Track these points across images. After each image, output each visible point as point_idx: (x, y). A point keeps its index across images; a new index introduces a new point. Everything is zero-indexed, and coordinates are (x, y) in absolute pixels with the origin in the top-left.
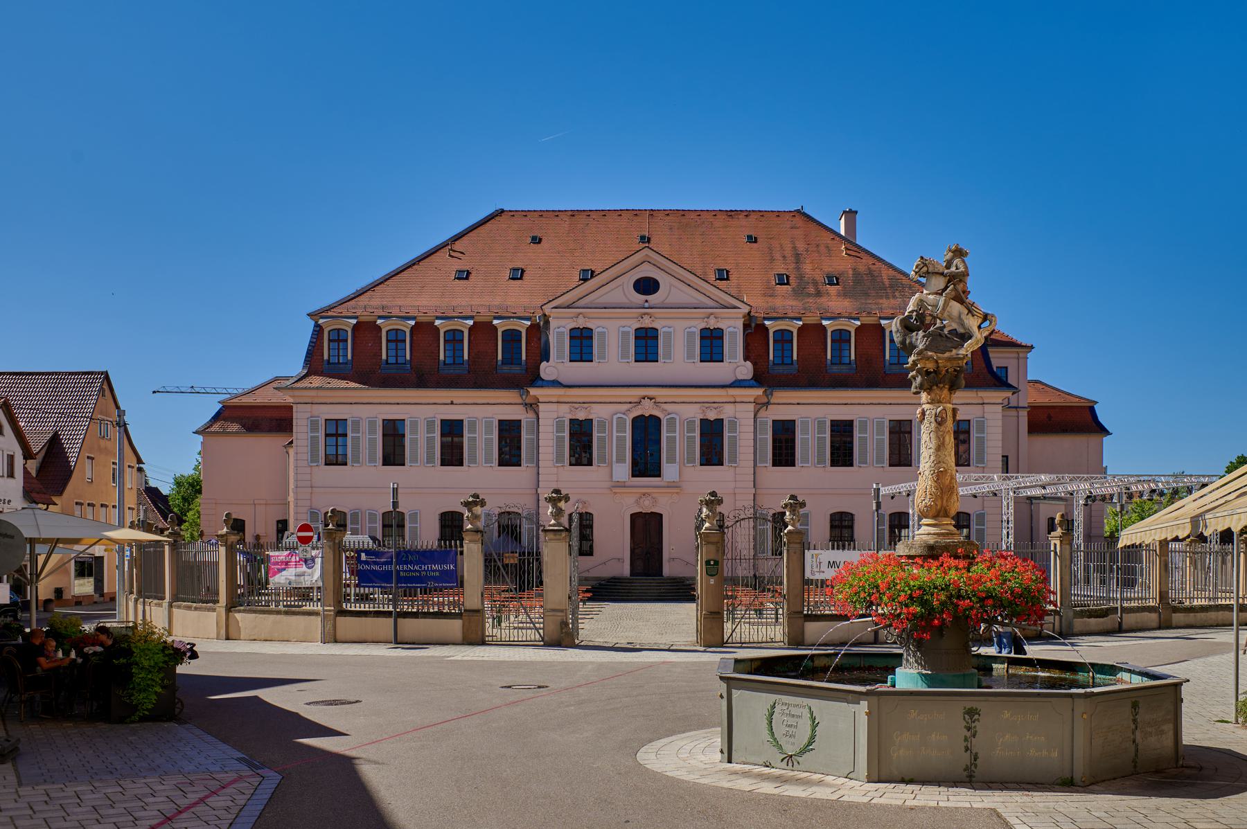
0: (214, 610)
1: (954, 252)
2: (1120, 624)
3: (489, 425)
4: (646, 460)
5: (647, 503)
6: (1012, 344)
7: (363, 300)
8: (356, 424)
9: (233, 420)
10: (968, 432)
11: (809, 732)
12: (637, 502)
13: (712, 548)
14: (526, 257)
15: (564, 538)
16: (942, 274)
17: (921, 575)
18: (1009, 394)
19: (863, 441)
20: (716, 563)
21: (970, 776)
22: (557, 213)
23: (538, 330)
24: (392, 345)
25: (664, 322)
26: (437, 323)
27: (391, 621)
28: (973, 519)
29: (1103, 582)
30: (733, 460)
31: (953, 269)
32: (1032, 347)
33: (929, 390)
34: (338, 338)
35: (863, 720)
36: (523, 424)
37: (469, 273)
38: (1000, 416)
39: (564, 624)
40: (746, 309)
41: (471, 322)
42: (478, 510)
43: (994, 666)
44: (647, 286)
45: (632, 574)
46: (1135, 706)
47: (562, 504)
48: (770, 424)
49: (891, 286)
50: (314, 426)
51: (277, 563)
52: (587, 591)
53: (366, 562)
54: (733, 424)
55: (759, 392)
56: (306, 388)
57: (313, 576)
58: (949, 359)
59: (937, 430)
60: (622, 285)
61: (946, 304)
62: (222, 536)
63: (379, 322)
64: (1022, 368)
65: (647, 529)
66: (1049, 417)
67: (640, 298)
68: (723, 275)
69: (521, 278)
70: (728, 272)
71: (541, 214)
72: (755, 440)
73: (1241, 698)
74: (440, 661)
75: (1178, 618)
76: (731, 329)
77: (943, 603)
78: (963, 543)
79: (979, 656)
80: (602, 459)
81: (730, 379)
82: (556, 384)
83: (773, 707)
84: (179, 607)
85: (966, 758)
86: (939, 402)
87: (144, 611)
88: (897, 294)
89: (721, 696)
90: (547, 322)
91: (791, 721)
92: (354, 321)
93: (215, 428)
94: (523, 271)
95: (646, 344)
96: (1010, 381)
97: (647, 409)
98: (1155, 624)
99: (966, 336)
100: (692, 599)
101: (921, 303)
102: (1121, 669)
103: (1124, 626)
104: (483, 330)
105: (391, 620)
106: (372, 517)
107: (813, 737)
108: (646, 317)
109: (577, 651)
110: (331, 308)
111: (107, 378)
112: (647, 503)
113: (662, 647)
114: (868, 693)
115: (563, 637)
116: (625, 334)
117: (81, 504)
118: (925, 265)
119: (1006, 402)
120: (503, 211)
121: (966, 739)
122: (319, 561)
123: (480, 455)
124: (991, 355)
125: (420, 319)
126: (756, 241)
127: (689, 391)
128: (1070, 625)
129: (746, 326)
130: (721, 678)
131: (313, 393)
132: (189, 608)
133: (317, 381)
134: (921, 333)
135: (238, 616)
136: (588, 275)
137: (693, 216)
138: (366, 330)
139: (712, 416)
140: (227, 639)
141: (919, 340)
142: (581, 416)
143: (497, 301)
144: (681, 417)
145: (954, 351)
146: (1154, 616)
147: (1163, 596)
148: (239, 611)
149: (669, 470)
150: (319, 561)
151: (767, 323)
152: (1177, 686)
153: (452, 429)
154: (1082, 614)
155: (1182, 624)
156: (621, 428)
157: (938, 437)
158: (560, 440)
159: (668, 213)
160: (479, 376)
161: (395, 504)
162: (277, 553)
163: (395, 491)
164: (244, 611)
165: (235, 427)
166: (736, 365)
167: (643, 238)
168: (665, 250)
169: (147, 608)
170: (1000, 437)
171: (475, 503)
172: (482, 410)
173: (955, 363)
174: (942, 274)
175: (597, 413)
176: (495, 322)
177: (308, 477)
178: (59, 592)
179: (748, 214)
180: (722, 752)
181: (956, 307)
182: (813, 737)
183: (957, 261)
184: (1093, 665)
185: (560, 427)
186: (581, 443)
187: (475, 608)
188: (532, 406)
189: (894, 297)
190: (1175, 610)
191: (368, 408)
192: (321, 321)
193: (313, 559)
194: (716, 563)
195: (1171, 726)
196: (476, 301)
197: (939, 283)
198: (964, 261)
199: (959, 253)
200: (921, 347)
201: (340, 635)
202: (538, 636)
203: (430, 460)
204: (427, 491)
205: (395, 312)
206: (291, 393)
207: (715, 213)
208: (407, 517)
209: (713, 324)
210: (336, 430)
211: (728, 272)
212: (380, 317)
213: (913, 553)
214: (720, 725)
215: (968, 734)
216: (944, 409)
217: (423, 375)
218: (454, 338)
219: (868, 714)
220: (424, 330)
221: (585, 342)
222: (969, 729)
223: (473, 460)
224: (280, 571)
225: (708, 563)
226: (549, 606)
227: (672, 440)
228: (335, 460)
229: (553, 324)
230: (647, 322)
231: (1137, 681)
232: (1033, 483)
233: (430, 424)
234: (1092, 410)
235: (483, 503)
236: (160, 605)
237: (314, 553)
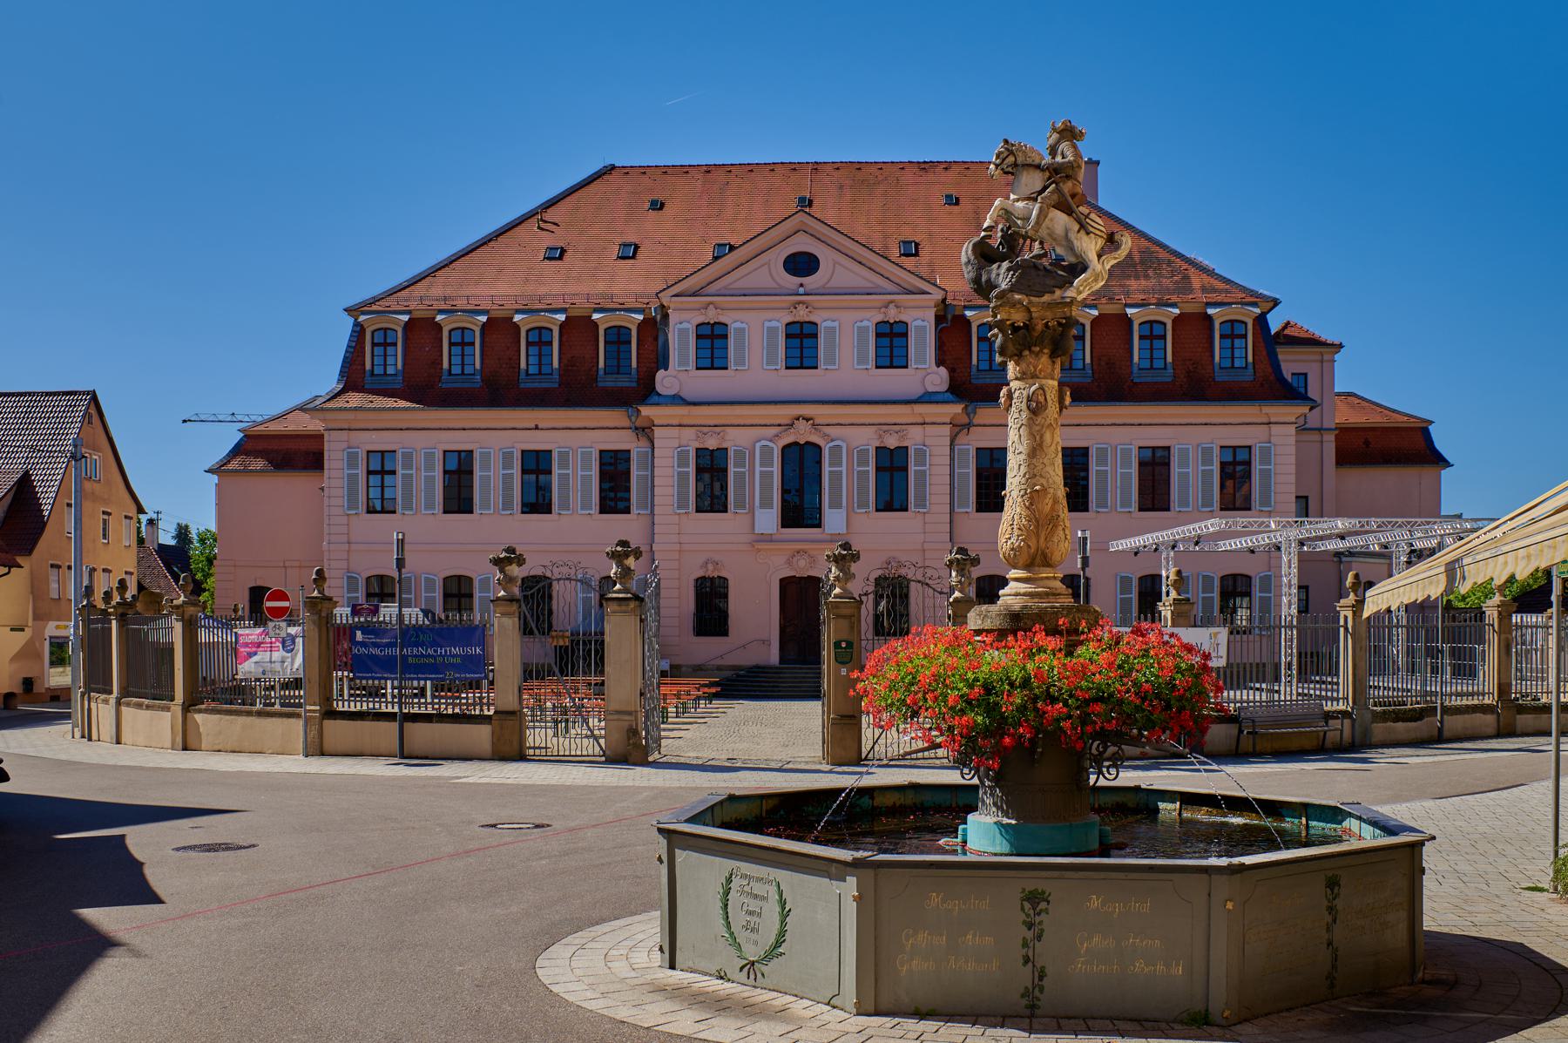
0: (168, 709)
1: (1061, 132)
2: (1440, 730)
3: (586, 457)
4: (799, 509)
5: (802, 563)
6: (1313, 342)
7: (419, 290)
8: (408, 457)
9: (257, 454)
10: (1248, 463)
11: (777, 926)
12: (789, 562)
13: (844, 623)
14: (646, 230)
15: (633, 610)
16: (1038, 167)
17: (995, 660)
18: (1305, 410)
19: (1102, 476)
20: (850, 644)
21: (1033, 1007)
22: (685, 170)
23: (654, 328)
24: (457, 350)
25: (825, 314)
26: (517, 318)
27: (395, 726)
28: (1256, 583)
29: (1435, 670)
30: (921, 502)
31: (1059, 159)
32: (1341, 346)
33: (1018, 357)
34: (384, 342)
35: (851, 908)
36: (634, 456)
37: (563, 251)
38: (1292, 440)
39: (633, 732)
40: (939, 295)
41: (562, 317)
42: (514, 570)
43: (1162, 805)
44: (802, 264)
45: (781, 661)
46: (1333, 883)
47: (631, 562)
48: (972, 453)
49: (1142, 262)
50: (352, 460)
51: (246, 645)
52: (711, 685)
53: (363, 644)
54: (921, 454)
55: (957, 409)
56: (340, 409)
57: (294, 663)
58: (1049, 306)
59: (1030, 424)
60: (768, 263)
61: (1042, 214)
62: (177, 607)
63: (439, 318)
64: (1327, 375)
65: (800, 596)
66: (1367, 443)
67: (792, 281)
68: (911, 250)
69: (634, 257)
70: (917, 245)
71: (666, 170)
72: (952, 475)
73: (1562, 853)
74: (439, 782)
75: (1524, 720)
76: (919, 323)
77: (1022, 709)
78: (1069, 609)
79: (1097, 790)
80: (740, 504)
81: (916, 390)
82: (678, 400)
83: (729, 880)
84: (128, 705)
85: (1025, 976)
86: (1034, 376)
87: (89, 710)
88: (1150, 272)
89: (660, 859)
90: (666, 316)
91: (754, 905)
92: (406, 318)
93: (234, 465)
94: (637, 247)
95: (802, 343)
96: (1310, 394)
97: (803, 433)
98: (1491, 731)
99: (1079, 267)
100: (814, 694)
101: (1007, 214)
102: (1350, 815)
103: (1446, 734)
104: (578, 327)
105: (395, 726)
106: (430, 584)
107: (782, 933)
108: (800, 307)
109: (646, 770)
110: (375, 300)
111: (94, 399)
112: (802, 563)
113: (773, 765)
114: (857, 864)
115: (631, 750)
116: (772, 331)
117: (59, 567)
118: (1011, 153)
119: (1301, 421)
120: (613, 167)
121: (1025, 944)
122: (299, 641)
123: (576, 498)
124: (1280, 357)
125: (494, 314)
126: (957, 203)
127: (863, 401)
128: (1366, 732)
129: (939, 319)
130: (660, 830)
131: (350, 416)
132: (139, 706)
133: (355, 399)
134: (1005, 265)
135: (198, 717)
136: (723, 250)
137: (873, 170)
138: (422, 329)
139: (892, 442)
140: (185, 749)
141: (1002, 275)
142: (712, 443)
143: (601, 287)
144: (849, 446)
145: (1058, 293)
146: (1490, 719)
147: (1504, 689)
148: (200, 711)
149: (834, 520)
150: (299, 641)
151: (968, 313)
152: (1415, 848)
153: (536, 464)
154: (1384, 717)
155: (1530, 730)
156: (766, 461)
157: (1032, 435)
158: (683, 477)
159: (838, 166)
160: (575, 389)
161: (400, 563)
162: (247, 631)
163: (401, 543)
164: (206, 711)
165: (259, 464)
166: (925, 371)
167: (802, 200)
168: (831, 216)
169: (93, 705)
170: (1293, 469)
171: (509, 561)
172: (578, 438)
173: (1059, 312)
174: (1038, 167)
175: (735, 440)
176: (595, 316)
177: (344, 529)
178: (28, 683)
179: (948, 166)
180: (661, 949)
181: (1060, 220)
182: (782, 933)
183: (1064, 146)
184: (1305, 806)
185: (683, 461)
186: (712, 481)
187: (510, 708)
188: (645, 431)
189: (1147, 277)
190: (1522, 710)
191: (425, 437)
192: (362, 318)
193: (293, 639)
194: (850, 644)
195: (1403, 914)
196: (572, 288)
197: (1032, 181)
198: (1075, 147)
199: (1069, 133)
200: (1003, 286)
201: (328, 744)
202: (597, 749)
203: (507, 505)
204: (438, 545)
205: (461, 304)
206: (320, 415)
207: (903, 166)
208: (476, 584)
209: (893, 315)
210: (381, 467)
211: (917, 245)
212: (441, 312)
213: (988, 625)
214: (660, 907)
215: (1029, 935)
216: (1041, 388)
217: (499, 390)
218: (540, 339)
219: (859, 899)
220: (499, 328)
221: (718, 343)
222: (1030, 926)
223: (565, 505)
224: (250, 655)
225: (837, 645)
226: (613, 706)
227: (836, 477)
228: (382, 507)
229: (673, 317)
230: (802, 314)
231: (1369, 837)
232: (1332, 531)
233: (507, 458)
234: (1425, 433)
235: (520, 561)
236: (106, 702)
237: (293, 630)
